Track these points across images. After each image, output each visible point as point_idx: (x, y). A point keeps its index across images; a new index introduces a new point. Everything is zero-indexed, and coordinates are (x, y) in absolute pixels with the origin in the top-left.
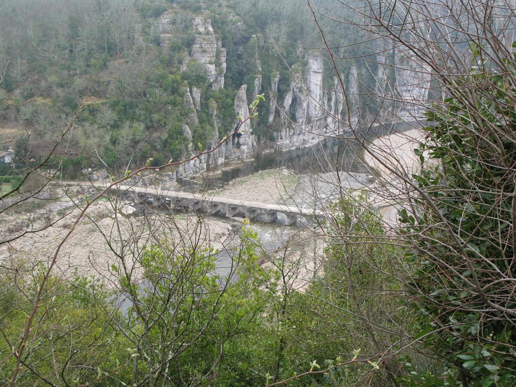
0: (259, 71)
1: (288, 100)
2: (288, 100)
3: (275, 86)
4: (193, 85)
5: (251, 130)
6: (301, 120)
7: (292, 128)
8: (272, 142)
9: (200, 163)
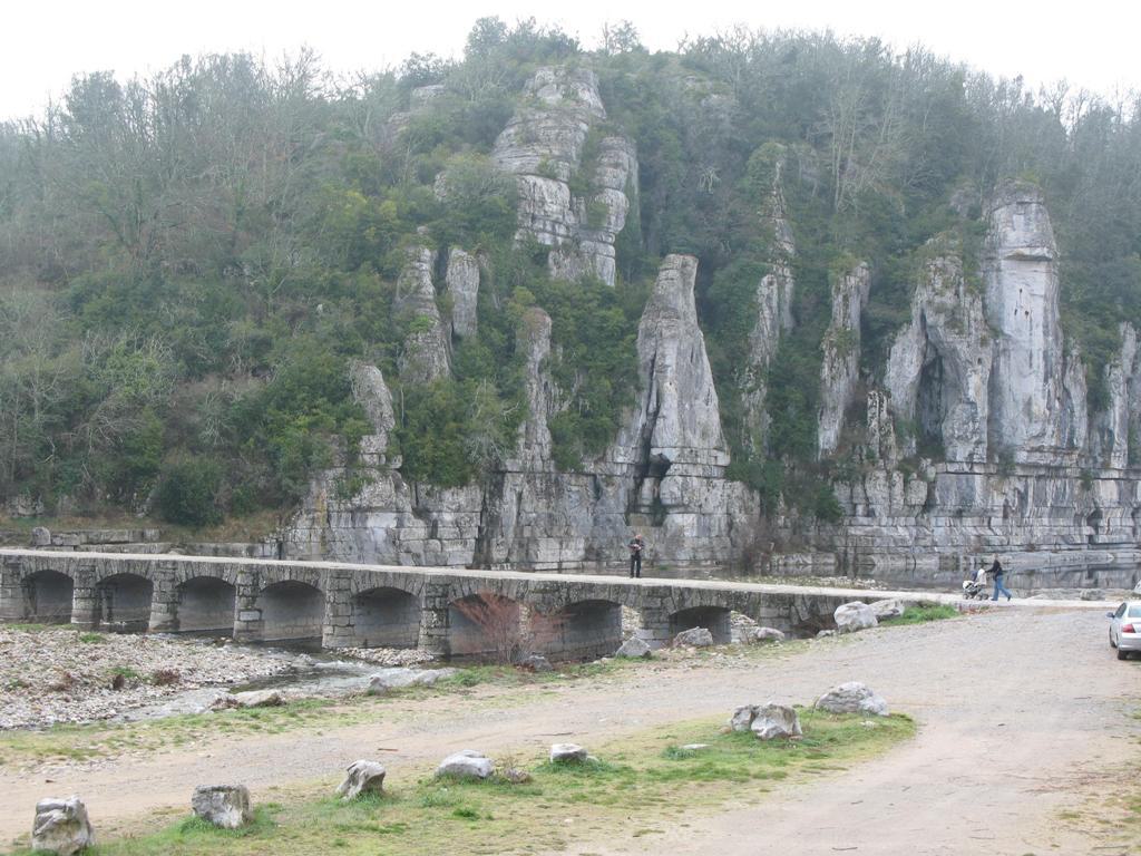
0: (784, 255)
1: (904, 364)
2: (904, 364)
3: (846, 306)
4: (456, 240)
5: (724, 459)
6: (961, 452)
7: (922, 476)
8: (829, 527)
9: (433, 535)
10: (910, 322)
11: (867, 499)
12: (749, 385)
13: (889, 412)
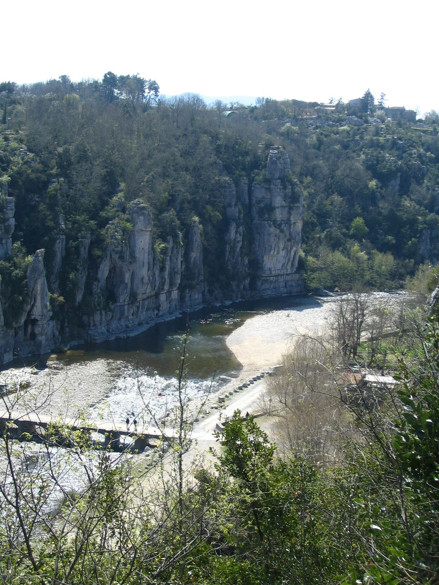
10: (107, 257)
11: (94, 321)
12: (54, 281)
13: (100, 289)
